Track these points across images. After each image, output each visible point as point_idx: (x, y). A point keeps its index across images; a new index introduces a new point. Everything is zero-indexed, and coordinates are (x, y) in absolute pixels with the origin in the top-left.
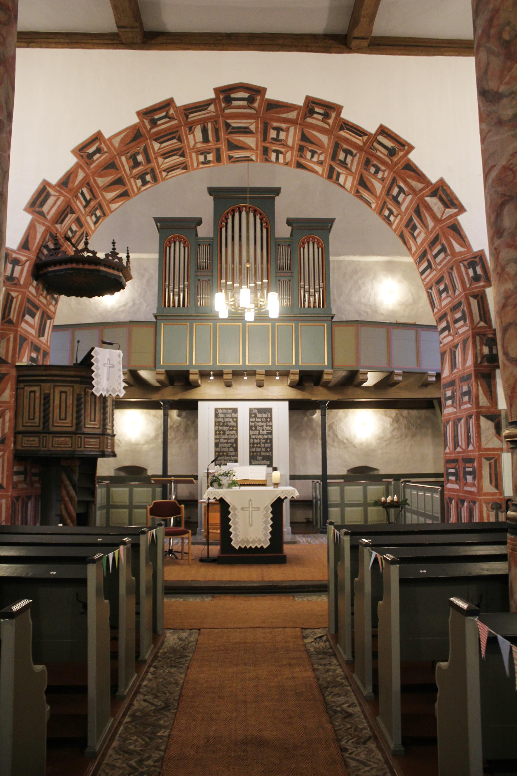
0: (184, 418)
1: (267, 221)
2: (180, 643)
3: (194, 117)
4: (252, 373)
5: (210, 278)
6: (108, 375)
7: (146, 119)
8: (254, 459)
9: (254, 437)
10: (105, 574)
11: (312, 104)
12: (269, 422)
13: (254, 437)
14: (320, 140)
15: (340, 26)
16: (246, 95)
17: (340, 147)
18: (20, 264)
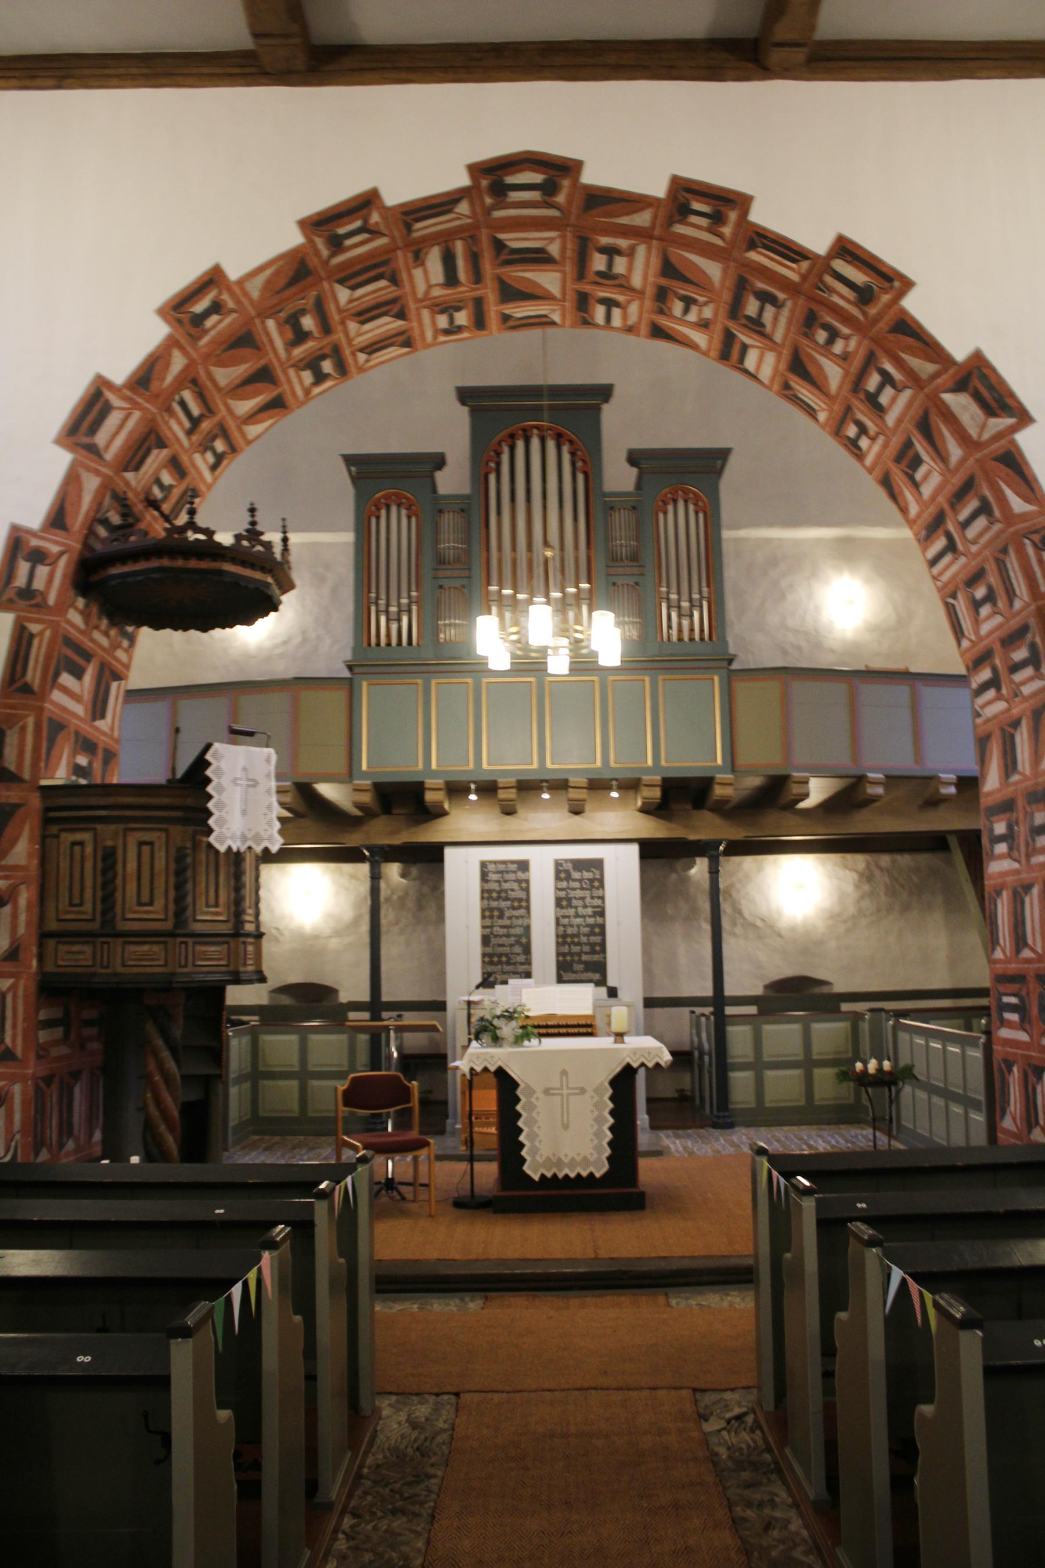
0: (414, 879)
1: (587, 460)
2: (415, 1434)
3: (424, 228)
4: (559, 785)
5: (465, 582)
6: (245, 799)
7: (319, 236)
8: (567, 970)
9: (565, 921)
10: (220, 1348)
11: (685, 194)
12: (598, 889)
13: (565, 921)
14: (704, 273)
15: (744, 18)
16: (537, 178)
17: (748, 287)
18: (48, 561)
